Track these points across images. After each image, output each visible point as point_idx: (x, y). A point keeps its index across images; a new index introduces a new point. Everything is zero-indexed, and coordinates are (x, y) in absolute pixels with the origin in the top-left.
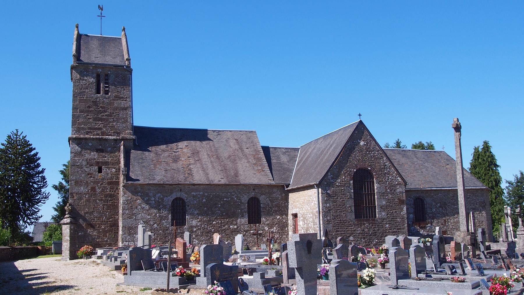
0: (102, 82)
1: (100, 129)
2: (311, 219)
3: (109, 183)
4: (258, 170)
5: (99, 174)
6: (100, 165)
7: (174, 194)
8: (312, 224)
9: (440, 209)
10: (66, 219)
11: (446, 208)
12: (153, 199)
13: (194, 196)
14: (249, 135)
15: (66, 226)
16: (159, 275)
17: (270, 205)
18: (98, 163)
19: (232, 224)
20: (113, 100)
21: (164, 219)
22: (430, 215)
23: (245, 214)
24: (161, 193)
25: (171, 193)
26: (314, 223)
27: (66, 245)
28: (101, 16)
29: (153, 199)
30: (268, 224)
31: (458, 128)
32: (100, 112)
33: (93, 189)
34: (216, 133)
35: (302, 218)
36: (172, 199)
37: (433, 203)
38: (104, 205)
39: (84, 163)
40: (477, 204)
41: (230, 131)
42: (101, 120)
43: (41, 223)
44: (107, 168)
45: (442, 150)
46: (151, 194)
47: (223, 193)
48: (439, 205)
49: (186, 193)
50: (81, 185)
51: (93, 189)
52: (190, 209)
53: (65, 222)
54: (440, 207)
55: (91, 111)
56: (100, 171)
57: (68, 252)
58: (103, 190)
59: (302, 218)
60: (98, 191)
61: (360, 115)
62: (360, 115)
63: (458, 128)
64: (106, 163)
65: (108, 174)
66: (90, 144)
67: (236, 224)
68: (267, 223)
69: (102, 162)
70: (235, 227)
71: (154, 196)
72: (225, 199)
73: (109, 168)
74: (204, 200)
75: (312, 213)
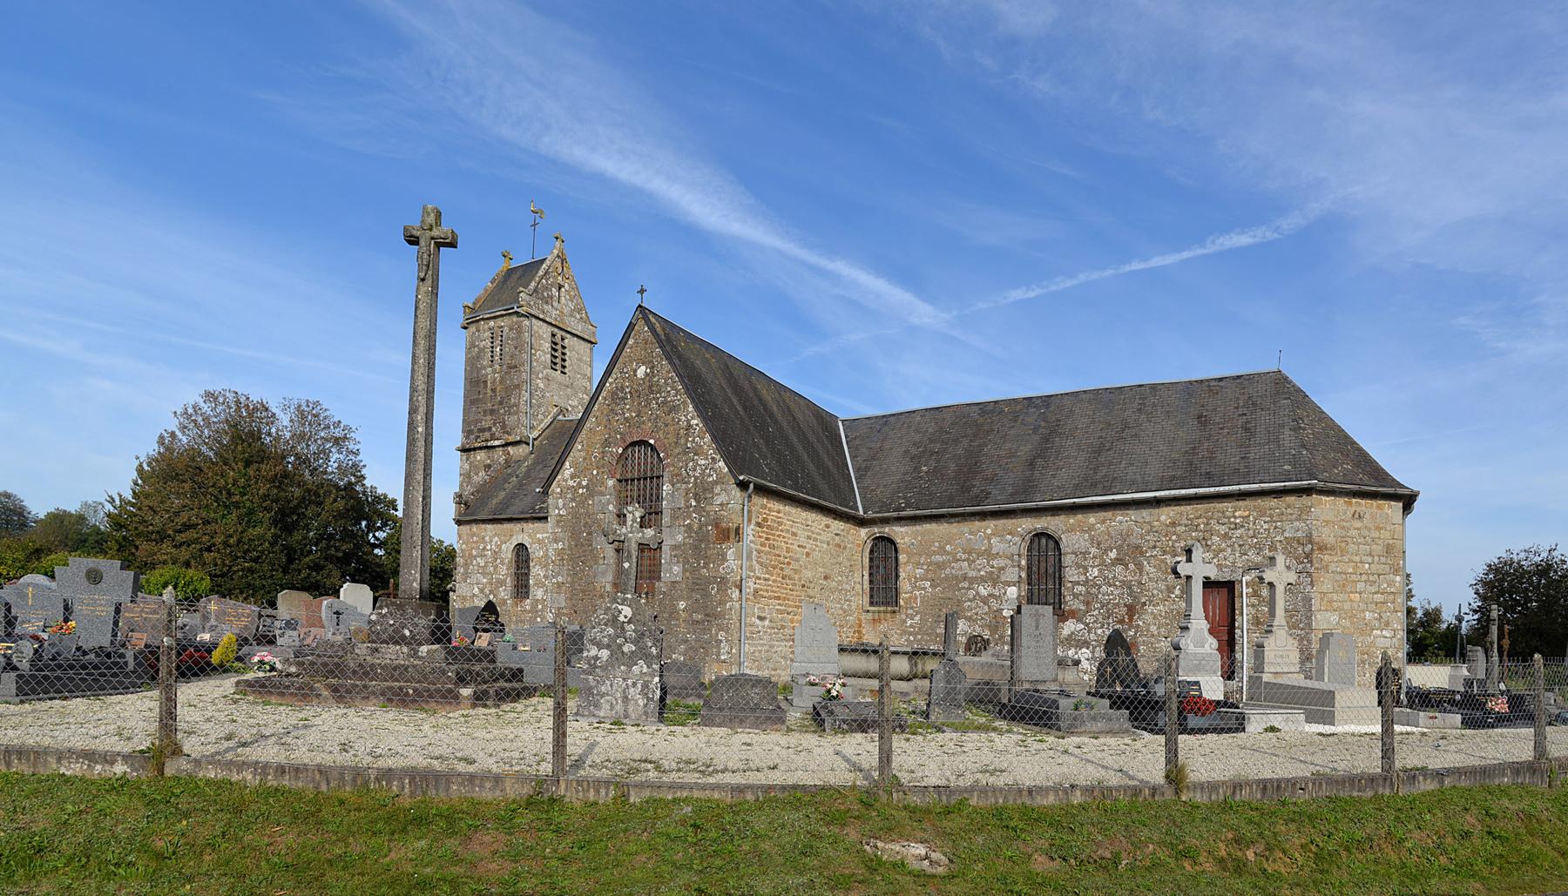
22: (1080, 589)
37: (1093, 550)
48: (1113, 554)
54: (1119, 561)
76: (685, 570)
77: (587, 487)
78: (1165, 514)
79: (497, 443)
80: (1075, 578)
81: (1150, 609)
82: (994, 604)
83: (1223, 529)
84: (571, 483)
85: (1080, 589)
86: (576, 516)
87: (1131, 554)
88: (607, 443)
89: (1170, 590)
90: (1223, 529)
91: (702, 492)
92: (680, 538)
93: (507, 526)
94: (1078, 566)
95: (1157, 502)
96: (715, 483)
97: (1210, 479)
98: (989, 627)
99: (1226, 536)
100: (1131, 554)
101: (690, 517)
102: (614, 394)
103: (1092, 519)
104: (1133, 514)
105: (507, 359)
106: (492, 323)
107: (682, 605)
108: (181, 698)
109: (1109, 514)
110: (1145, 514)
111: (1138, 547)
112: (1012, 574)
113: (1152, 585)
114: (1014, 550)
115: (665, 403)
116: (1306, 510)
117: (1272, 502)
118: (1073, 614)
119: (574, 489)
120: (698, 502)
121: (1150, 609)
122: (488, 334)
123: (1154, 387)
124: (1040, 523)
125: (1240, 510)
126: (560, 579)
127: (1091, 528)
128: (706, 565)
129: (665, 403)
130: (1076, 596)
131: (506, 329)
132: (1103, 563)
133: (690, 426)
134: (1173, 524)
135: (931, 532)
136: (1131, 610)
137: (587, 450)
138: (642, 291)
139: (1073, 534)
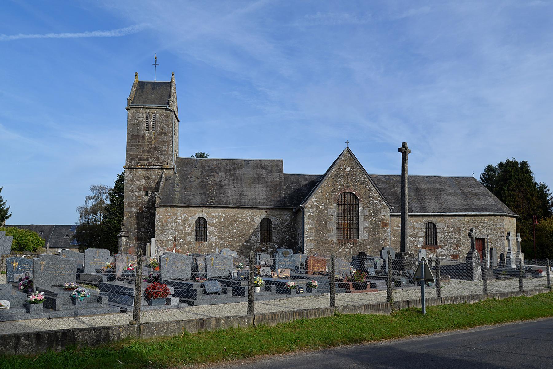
7: (198, 214)
9: (454, 233)
12: (180, 218)
13: (213, 216)
15: (524, 285)
16: (518, 248)
17: (281, 226)
18: (145, 188)
22: (442, 239)
24: (186, 213)
25: (195, 214)
29: (180, 218)
36: (196, 218)
37: (446, 228)
39: (135, 188)
40: (494, 230)
43: (7, 227)
45: (472, 176)
46: (179, 214)
47: (239, 214)
48: (452, 229)
49: (207, 214)
50: (132, 206)
54: (453, 231)
62: (347, 142)
66: (140, 173)
71: (181, 216)
74: (222, 220)
76: (369, 235)
77: (324, 206)
78: (466, 219)
79: (155, 167)
80: (441, 236)
81: (462, 245)
82: (415, 243)
83: (482, 224)
84: (316, 204)
85: (442, 239)
86: (319, 216)
87: (457, 230)
88: (333, 191)
89: (468, 240)
90: (482, 224)
91: (376, 211)
92: (367, 225)
93: (191, 209)
94: (442, 232)
95: (464, 216)
96: (382, 208)
97: (477, 210)
98: (414, 250)
99: (482, 226)
100: (457, 230)
101: (371, 218)
102: (335, 175)
103: (445, 219)
104: (457, 218)
105: (159, 129)
106: (148, 110)
107: (369, 247)
108: (488, 283)
109: (451, 218)
110: (461, 218)
111: (459, 228)
112: (422, 234)
113: (463, 238)
114: (422, 227)
115: (359, 181)
116: (502, 220)
117: (494, 218)
118: (440, 246)
120: (375, 214)
121: (462, 245)
122: (145, 115)
123: (439, 177)
124: (430, 219)
125: (486, 219)
126: (311, 238)
127: (445, 221)
128: (378, 234)
129: (359, 181)
130: (441, 241)
131: (158, 115)
132: (449, 232)
133: (370, 190)
134: (468, 222)
135: (394, 220)
136: (457, 245)
138: (347, 142)
139: (440, 223)
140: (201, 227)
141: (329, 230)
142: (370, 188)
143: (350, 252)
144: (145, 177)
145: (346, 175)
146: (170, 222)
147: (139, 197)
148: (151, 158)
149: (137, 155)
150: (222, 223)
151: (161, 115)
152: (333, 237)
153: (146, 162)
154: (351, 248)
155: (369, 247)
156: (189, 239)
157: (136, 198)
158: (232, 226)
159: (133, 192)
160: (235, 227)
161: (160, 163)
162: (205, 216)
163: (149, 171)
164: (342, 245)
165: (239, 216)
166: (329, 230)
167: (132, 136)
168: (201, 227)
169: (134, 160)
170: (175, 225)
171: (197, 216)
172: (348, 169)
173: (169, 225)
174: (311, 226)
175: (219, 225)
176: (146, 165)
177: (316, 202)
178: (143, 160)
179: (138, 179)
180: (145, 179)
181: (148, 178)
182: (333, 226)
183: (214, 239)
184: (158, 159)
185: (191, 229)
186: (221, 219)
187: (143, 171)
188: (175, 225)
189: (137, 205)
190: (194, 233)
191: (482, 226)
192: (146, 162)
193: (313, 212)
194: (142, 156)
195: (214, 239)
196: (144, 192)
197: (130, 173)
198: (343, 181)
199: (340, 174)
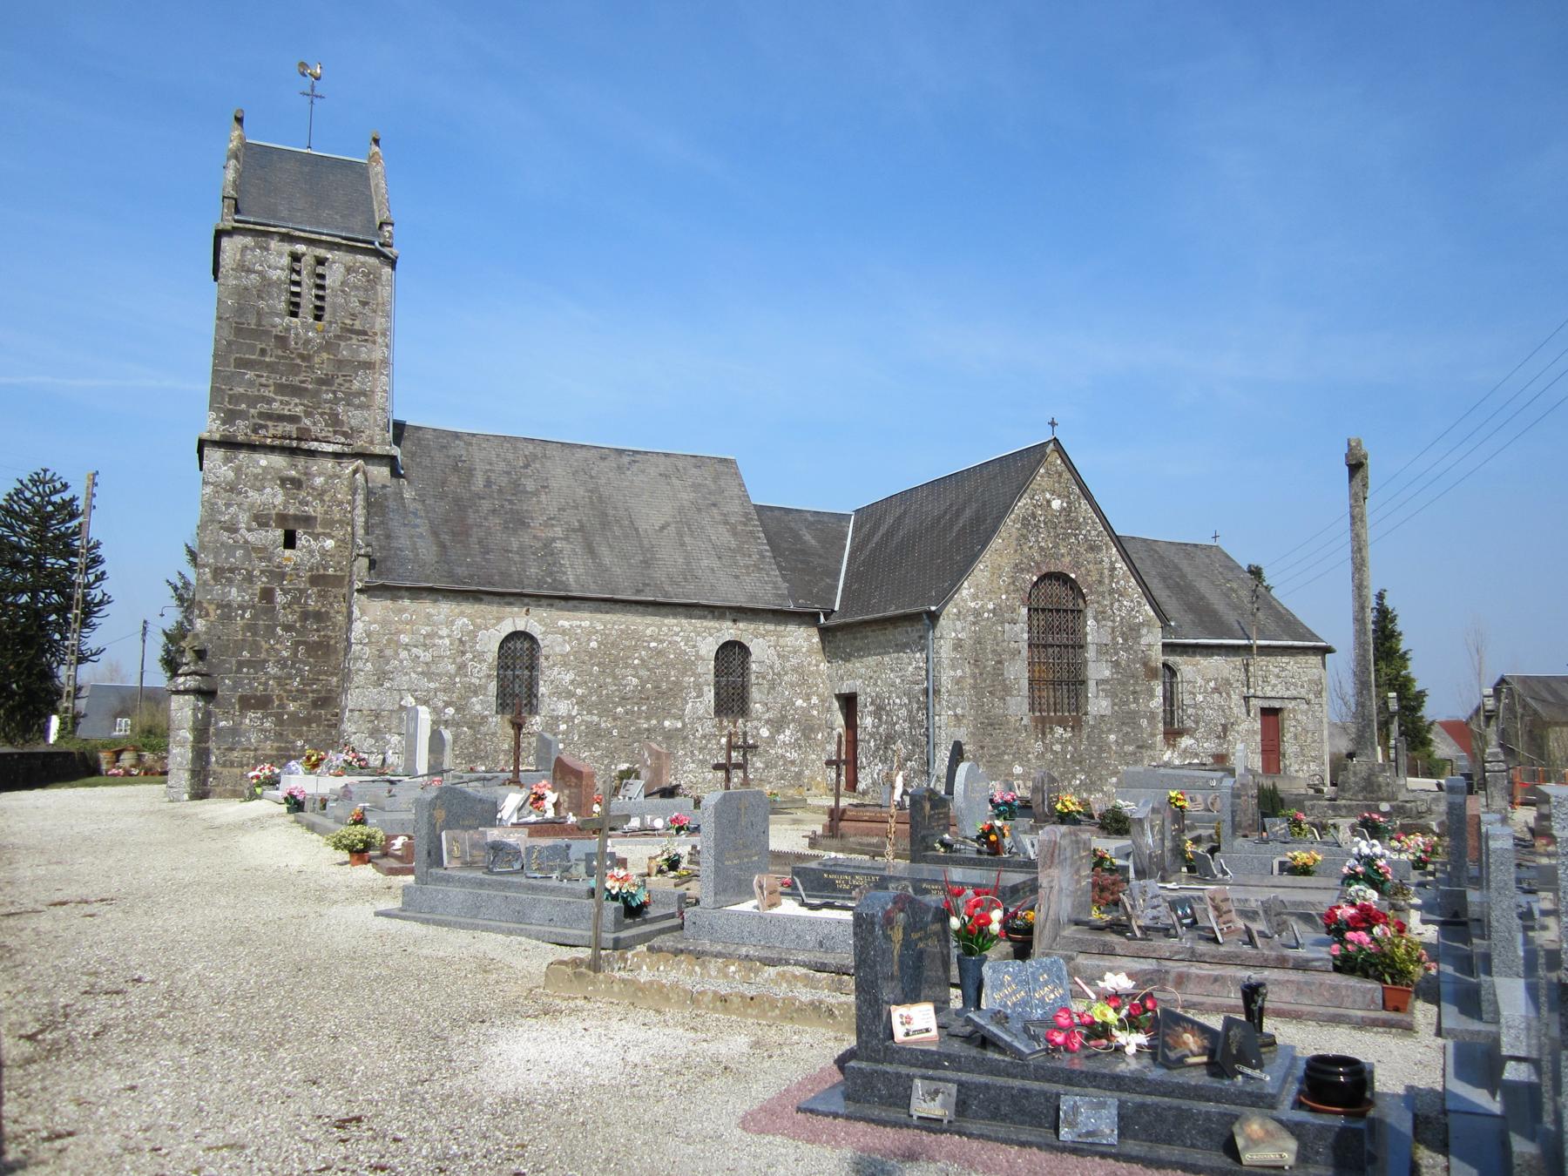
0: (302, 229)
1: (293, 419)
2: (903, 712)
3: (315, 580)
4: (747, 567)
5: (288, 552)
6: (291, 527)
8: (907, 725)
9: (1216, 696)
10: (182, 679)
11: (1229, 695)
14: (720, 468)
15: (181, 699)
18: (282, 519)
19: (669, 715)
20: (338, 337)
21: (476, 694)
23: (706, 689)
26: (911, 722)
27: (180, 755)
28: (312, 95)
30: (767, 722)
31: (1356, 467)
32: (295, 369)
33: (267, 594)
34: (612, 462)
35: (871, 708)
36: (504, 635)
38: (297, 643)
39: (244, 518)
41: (667, 455)
42: (296, 391)
44: (310, 534)
45: (1211, 542)
48: (1212, 684)
50: (230, 581)
51: (267, 594)
52: (550, 668)
53: (182, 688)
54: (1216, 690)
55: (269, 366)
56: (290, 541)
57: (187, 775)
58: (296, 600)
59: (871, 708)
60: (280, 598)
61: (1053, 424)
62: (1053, 424)
63: (1356, 467)
64: (307, 521)
65: (311, 552)
66: (263, 463)
67: (681, 718)
68: (766, 716)
69: (296, 518)
70: (679, 725)
72: (653, 644)
73: (316, 537)
74: (594, 644)
75: (908, 694)
92: (1107, 673)
102: (1025, 522)
107: (1112, 737)
119: (977, 613)
128: (1136, 701)
136: (1225, 727)
137: (997, 571)
140: (519, 655)
141: (1007, 690)
142: (1112, 563)
143: (1064, 751)
144: (284, 481)
145: (1051, 524)
146: (406, 647)
147: (255, 549)
148: (308, 414)
149: (253, 401)
150: (591, 655)
151: (349, 270)
152: (1018, 707)
153: (291, 428)
154: (1068, 741)
155: (1112, 737)
156: (478, 707)
157: (247, 555)
158: (627, 666)
159: (236, 531)
160: (635, 667)
161: (345, 434)
162: (536, 629)
163: (301, 461)
164: (1044, 734)
165: (648, 632)
166: (1007, 690)
167: (239, 331)
168: (519, 655)
169: (242, 415)
170: (425, 656)
171: (507, 628)
172: (1056, 504)
173: (404, 654)
174: (959, 672)
175: (580, 659)
176: (290, 438)
177: (975, 597)
178: (281, 418)
179: (259, 483)
180: (283, 485)
181: (297, 483)
182: (1018, 672)
183: (563, 707)
184: (335, 421)
185: (483, 672)
186: (589, 640)
187: (279, 461)
188: (425, 656)
189: (249, 578)
190: (493, 687)
191: (1278, 676)
192: (291, 428)
193: (963, 629)
194: (275, 405)
195: (563, 707)
196: (279, 534)
197: (227, 460)
198: (1044, 539)
199: (1034, 516)
